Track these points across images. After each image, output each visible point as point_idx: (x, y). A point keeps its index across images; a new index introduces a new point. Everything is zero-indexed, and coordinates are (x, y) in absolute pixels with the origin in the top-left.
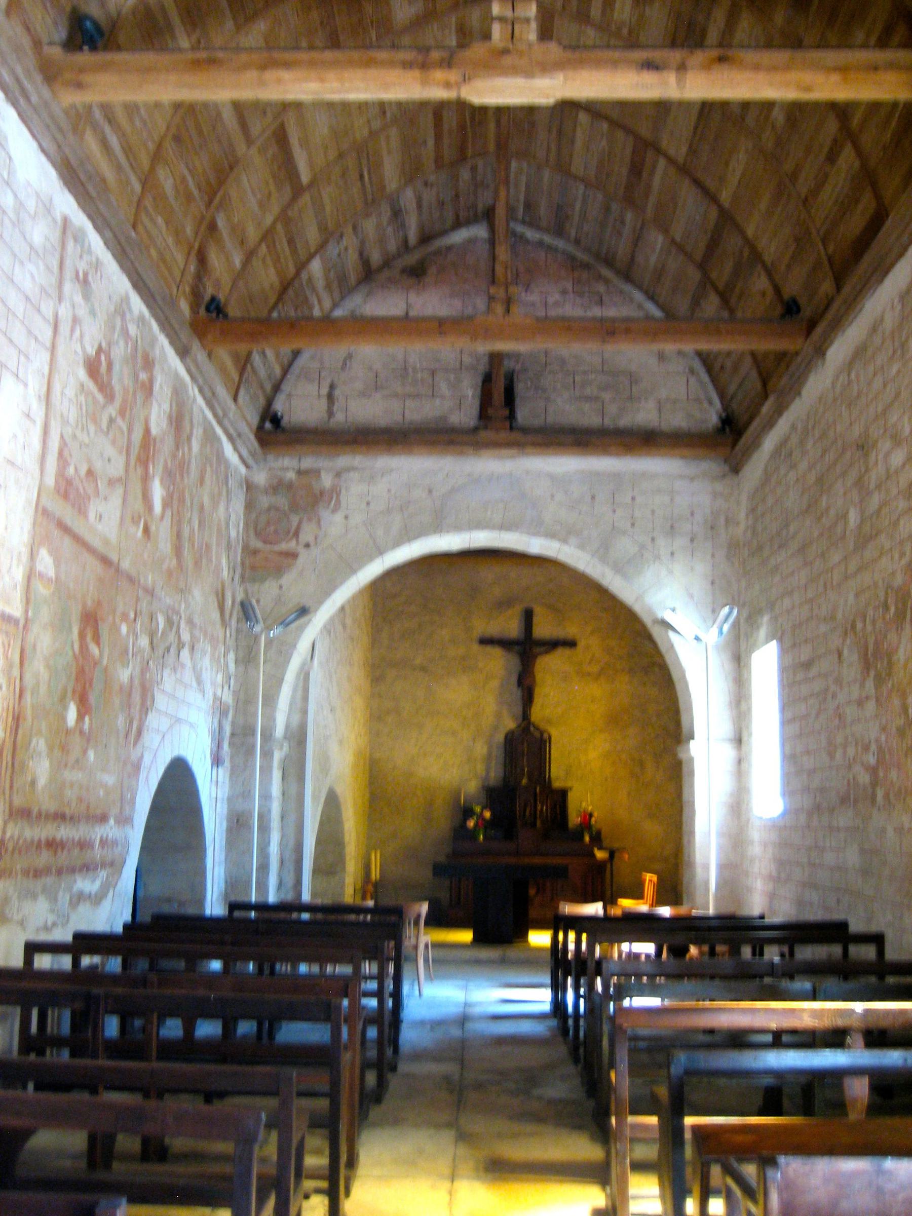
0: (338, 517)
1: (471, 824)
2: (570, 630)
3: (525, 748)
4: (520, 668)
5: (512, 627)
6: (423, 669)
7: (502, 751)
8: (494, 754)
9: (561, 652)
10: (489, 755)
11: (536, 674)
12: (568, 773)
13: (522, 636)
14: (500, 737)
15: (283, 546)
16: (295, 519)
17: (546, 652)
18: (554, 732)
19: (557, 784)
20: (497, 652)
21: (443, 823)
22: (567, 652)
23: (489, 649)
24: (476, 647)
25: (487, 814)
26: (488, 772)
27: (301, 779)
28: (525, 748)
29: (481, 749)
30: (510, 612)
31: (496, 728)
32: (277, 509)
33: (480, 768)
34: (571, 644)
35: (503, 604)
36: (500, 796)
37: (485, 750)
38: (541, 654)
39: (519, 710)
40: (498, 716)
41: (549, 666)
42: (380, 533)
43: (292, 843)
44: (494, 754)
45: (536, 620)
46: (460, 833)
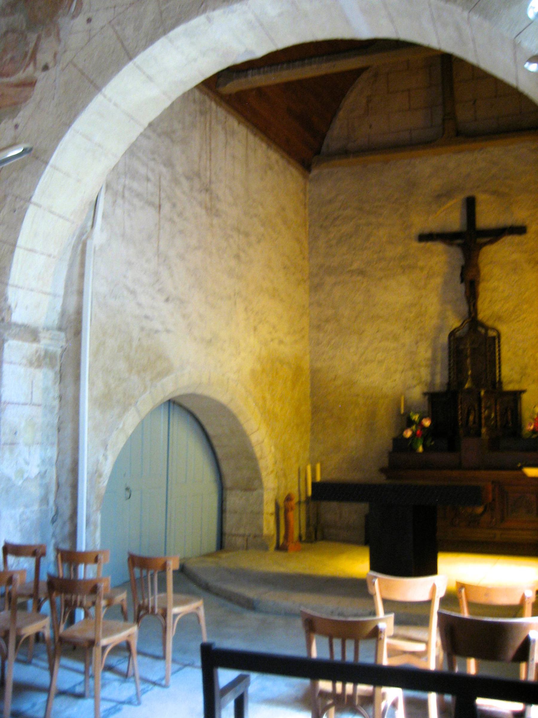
0: (80, 22)
1: (408, 434)
2: (519, 215)
3: (472, 348)
4: (462, 262)
5: (452, 219)
6: (361, 272)
7: (446, 352)
8: (439, 359)
9: (508, 239)
10: (434, 359)
11: (481, 265)
12: (523, 374)
13: (465, 229)
14: (444, 339)
15: (21, 76)
16: (32, 37)
17: (491, 242)
18: (503, 329)
19: (509, 387)
20: (439, 247)
21: (384, 437)
22: (516, 239)
23: (429, 244)
24: (416, 245)
25: (427, 423)
26: (433, 374)
27: (77, 378)
28: (472, 348)
29: (424, 353)
30: (451, 203)
31: (439, 329)
32: (14, 31)
33: (425, 373)
34: (519, 230)
35: (442, 196)
36: (440, 402)
37: (429, 354)
38: (485, 244)
39: (464, 308)
40: (442, 316)
41: (495, 259)
42: (129, 31)
43: (68, 461)
44: (439, 359)
45: (479, 208)
46: (400, 445)
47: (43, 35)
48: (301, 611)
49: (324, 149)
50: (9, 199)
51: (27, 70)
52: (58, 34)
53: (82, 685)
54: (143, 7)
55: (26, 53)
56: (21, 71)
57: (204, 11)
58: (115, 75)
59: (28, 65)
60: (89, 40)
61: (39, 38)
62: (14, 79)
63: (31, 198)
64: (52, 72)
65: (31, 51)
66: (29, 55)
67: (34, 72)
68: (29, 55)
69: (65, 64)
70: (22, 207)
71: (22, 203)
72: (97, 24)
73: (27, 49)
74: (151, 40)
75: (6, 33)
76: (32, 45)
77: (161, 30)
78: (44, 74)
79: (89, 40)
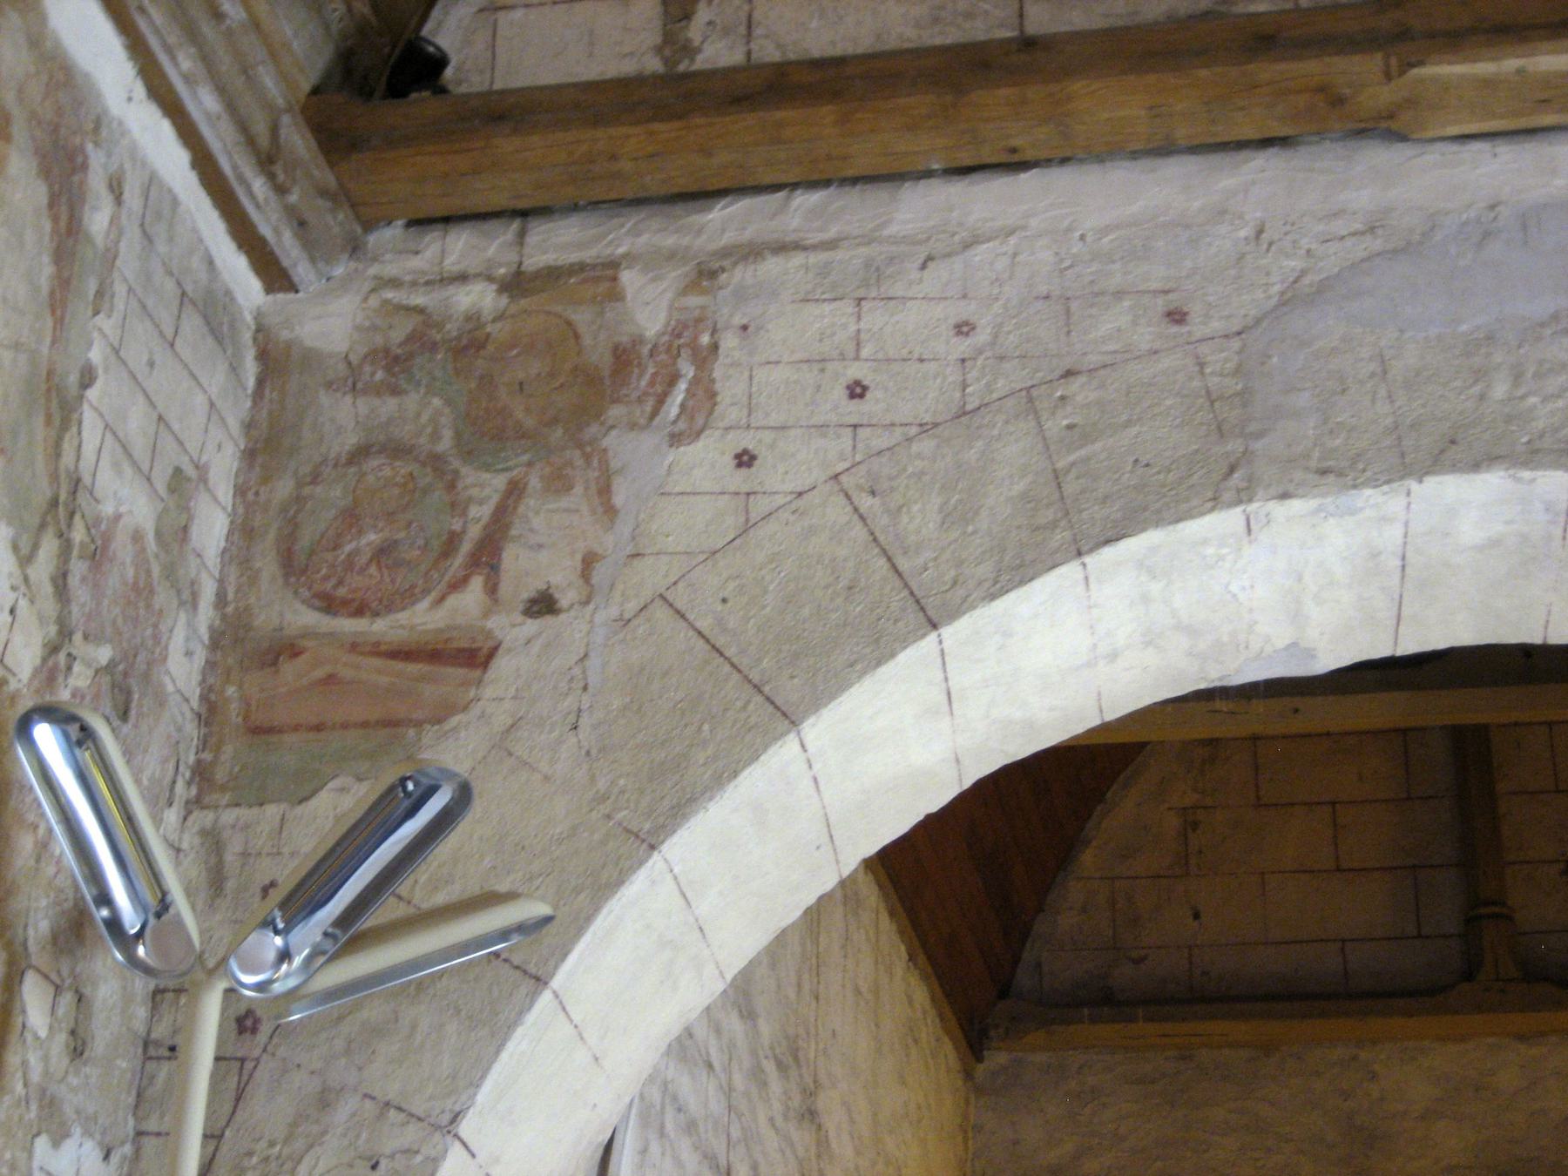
0: (705, 459)
15: (423, 618)
16: (484, 488)
32: (397, 450)
47: (534, 482)
48: (332, 165)
49: (1024, 979)
50: (343, 1112)
51: (452, 601)
52: (605, 490)
53: (754, 517)
54: (979, 444)
55: (451, 542)
56: (424, 605)
57: (1244, 496)
58: (863, 673)
59: (458, 585)
60: (747, 528)
61: (515, 490)
62: (381, 627)
63: (456, 1118)
64: (572, 627)
65: (474, 532)
66: (466, 547)
67: (486, 614)
68: (466, 547)
69: (632, 607)
70: (410, 1152)
71: (411, 1134)
72: (784, 472)
73: (457, 525)
74: (1016, 570)
75: (360, 453)
76: (481, 513)
77: (1060, 536)
78: (532, 626)
79: (747, 528)
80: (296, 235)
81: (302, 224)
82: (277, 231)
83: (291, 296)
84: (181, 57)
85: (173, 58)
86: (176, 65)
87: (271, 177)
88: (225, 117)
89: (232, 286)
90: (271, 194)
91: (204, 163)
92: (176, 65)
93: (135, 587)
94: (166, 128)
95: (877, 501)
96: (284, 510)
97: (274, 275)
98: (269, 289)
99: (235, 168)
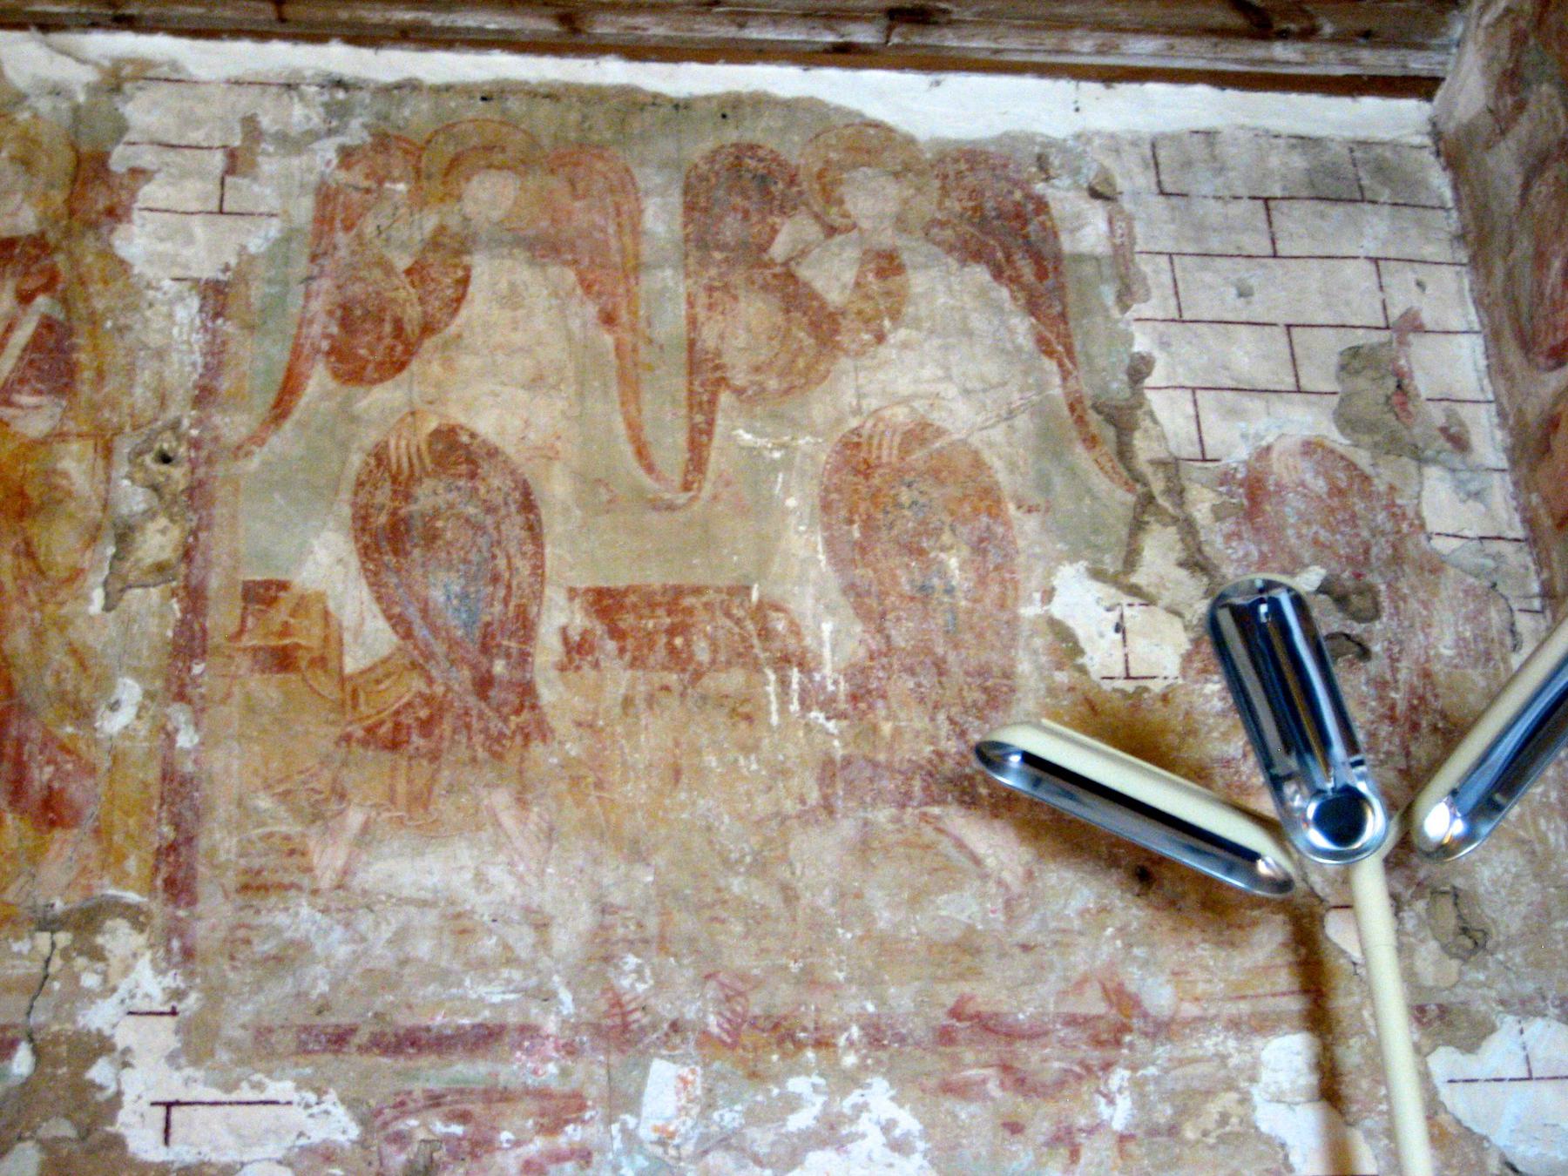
78: (1413, 285)
80: (1374, 46)
81: (1367, 34)
82: (1346, 62)
83: (1444, 85)
84: (1076, 46)
85: (1071, 52)
86: (1079, 54)
87: (1284, 35)
88: (1176, 41)
89: (1348, 134)
90: (1301, 46)
91: (1220, 80)
92: (1079, 54)
93: (1336, 491)
94: (1156, 90)
95: (269, 165)
96: (1505, 292)
97: (1423, 87)
98: (1428, 96)
99: (1236, 61)
